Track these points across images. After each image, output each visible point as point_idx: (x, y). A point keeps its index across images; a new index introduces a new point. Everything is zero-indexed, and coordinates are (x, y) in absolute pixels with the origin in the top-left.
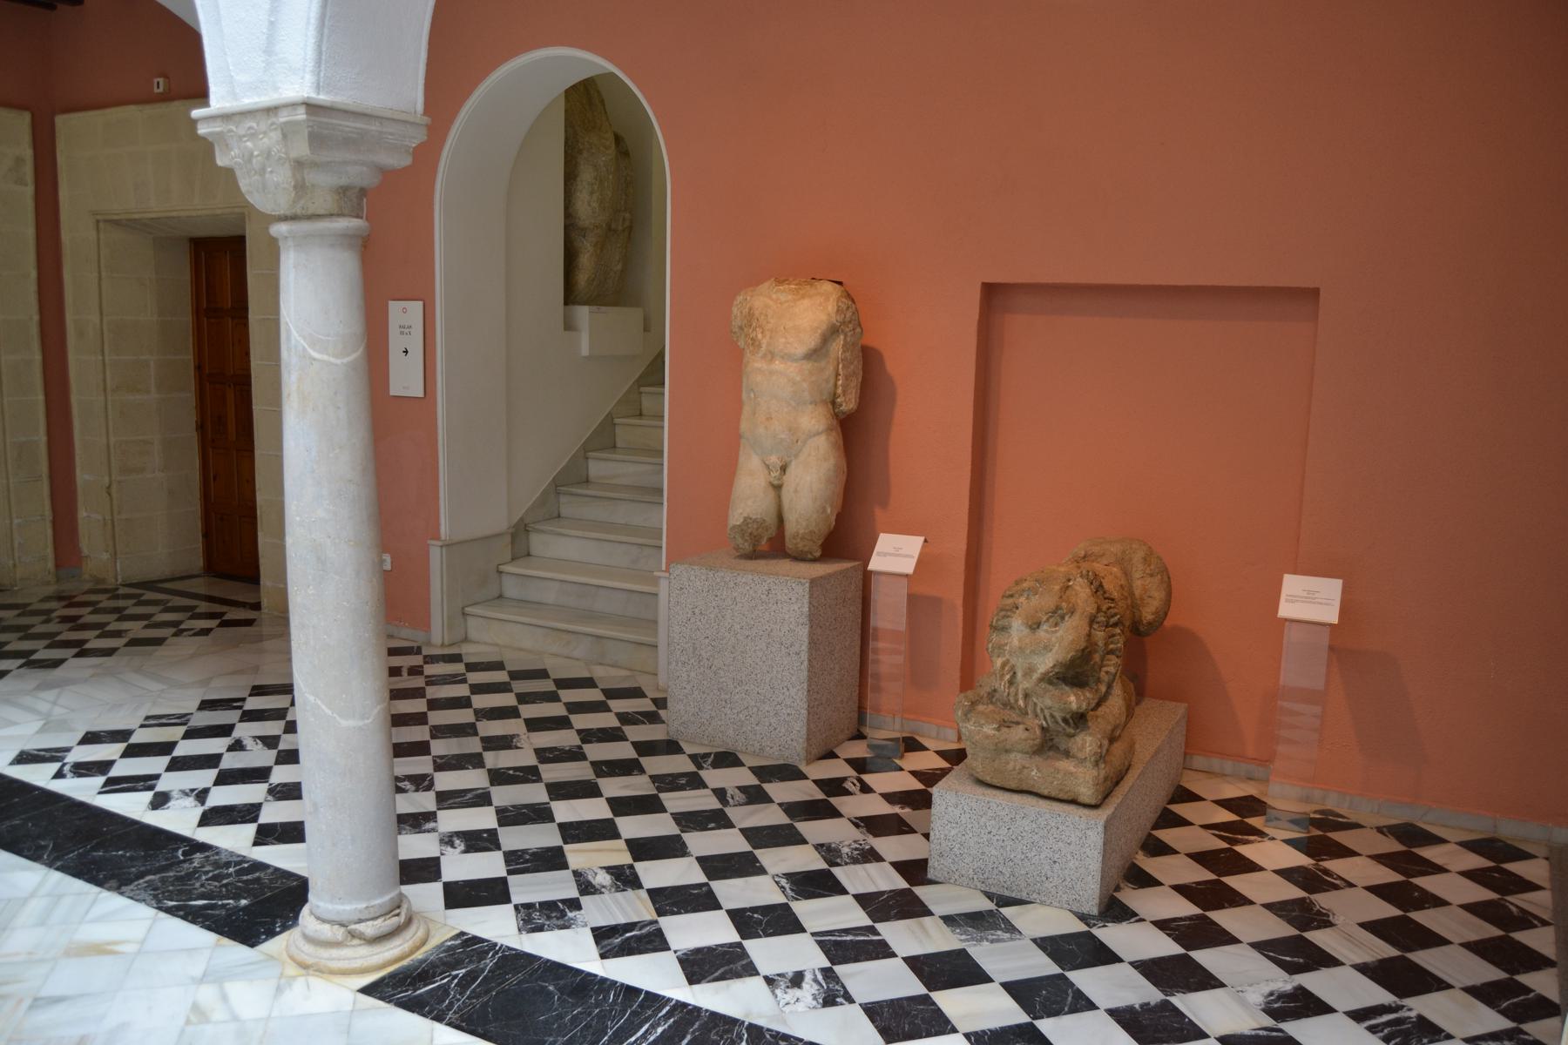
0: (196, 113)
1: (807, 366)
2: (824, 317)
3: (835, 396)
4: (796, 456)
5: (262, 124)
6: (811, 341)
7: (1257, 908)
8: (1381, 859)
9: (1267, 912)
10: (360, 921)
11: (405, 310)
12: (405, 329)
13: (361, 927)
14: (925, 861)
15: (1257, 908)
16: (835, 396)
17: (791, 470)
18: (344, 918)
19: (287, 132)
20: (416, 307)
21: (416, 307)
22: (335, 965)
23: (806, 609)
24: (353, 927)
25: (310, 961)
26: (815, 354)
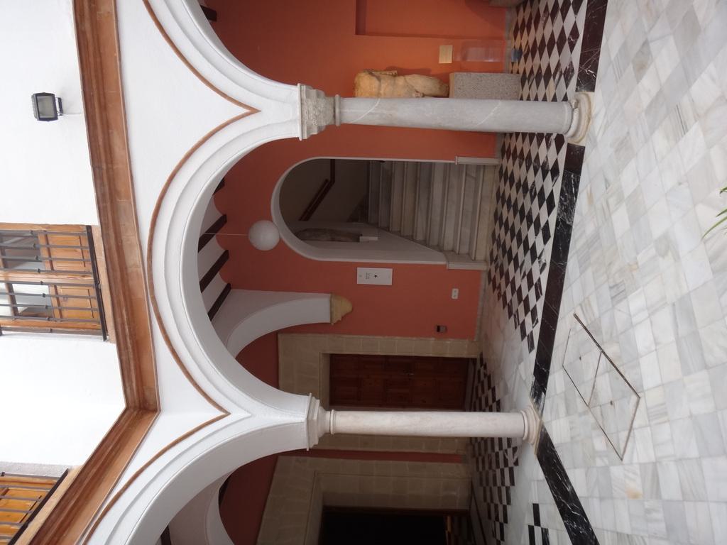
0: (300, 139)
1: (382, 81)
2: (366, 77)
3: (392, 75)
4: (413, 87)
5: (305, 107)
6: (374, 79)
7: (556, 156)
8: (539, 145)
9: (561, 29)
10: (571, 106)
11: (361, 276)
12: (368, 277)
13: (573, 104)
14: (534, 504)
15: (556, 156)
16: (392, 75)
17: (417, 89)
18: (571, 110)
19: (308, 96)
20: (360, 271)
21: (359, 269)
22: (585, 130)
23: (465, 74)
24: (573, 107)
25: (587, 117)
26: (379, 79)
